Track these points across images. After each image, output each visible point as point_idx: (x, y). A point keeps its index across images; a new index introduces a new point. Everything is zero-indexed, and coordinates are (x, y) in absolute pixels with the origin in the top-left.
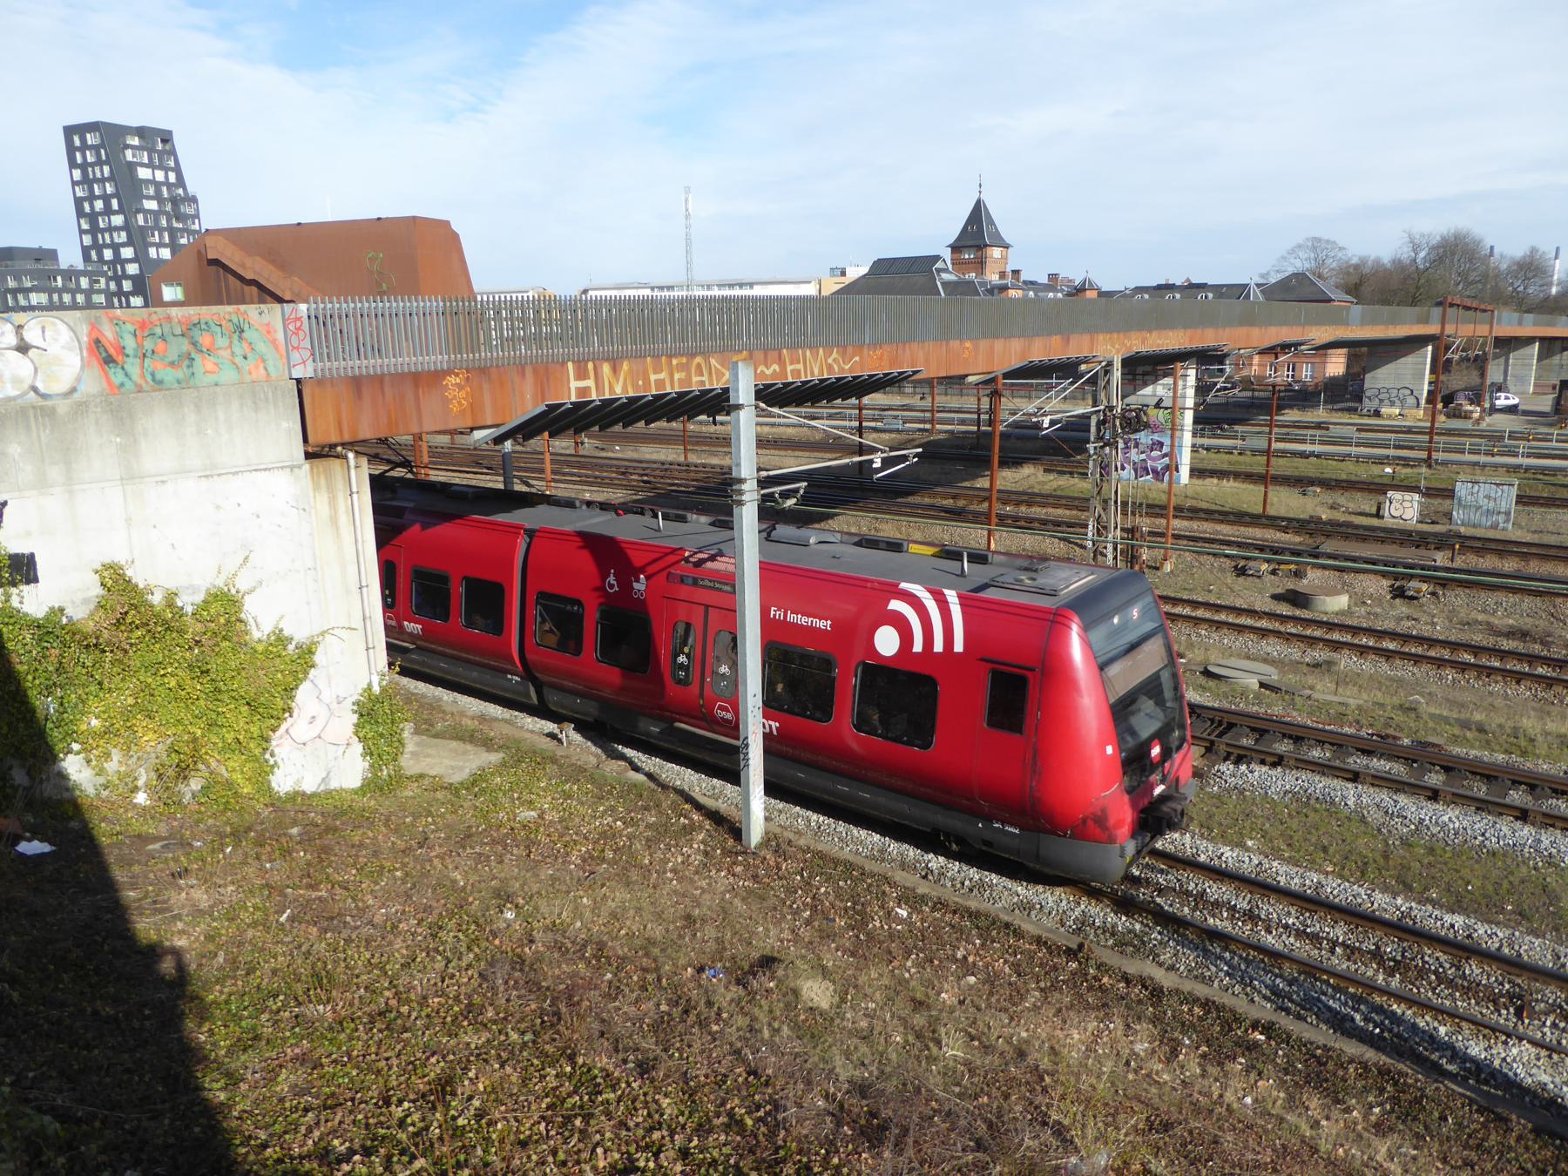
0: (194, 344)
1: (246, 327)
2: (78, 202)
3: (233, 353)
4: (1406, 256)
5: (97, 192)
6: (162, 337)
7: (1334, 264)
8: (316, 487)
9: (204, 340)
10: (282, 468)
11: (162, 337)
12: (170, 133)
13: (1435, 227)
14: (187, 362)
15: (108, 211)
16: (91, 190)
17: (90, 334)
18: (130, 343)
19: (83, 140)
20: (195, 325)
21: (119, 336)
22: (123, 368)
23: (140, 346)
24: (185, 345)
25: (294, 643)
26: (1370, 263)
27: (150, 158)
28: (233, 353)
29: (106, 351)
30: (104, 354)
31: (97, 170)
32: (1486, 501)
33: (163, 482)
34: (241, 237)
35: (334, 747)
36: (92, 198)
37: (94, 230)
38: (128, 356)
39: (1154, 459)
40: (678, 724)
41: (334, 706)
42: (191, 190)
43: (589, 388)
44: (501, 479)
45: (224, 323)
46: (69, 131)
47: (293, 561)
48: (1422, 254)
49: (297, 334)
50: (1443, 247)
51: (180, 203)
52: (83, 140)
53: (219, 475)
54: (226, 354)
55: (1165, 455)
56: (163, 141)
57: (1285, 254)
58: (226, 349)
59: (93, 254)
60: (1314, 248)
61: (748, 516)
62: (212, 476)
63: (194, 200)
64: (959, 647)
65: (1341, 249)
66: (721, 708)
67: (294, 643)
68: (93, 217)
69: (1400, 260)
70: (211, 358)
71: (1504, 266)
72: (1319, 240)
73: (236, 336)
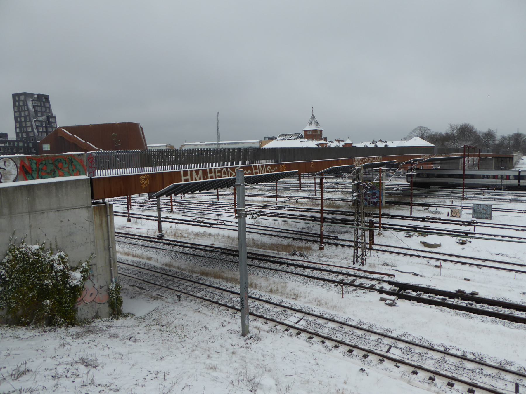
0: (56, 167)
1: (74, 161)
2: (16, 118)
3: (69, 169)
4: (450, 132)
5: (22, 114)
6: (45, 165)
7: (427, 135)
8: (95, 214)
9: (59, 165)
10: (84, 207)
11: (45, 165)
12: (48, 96)
13: (460, 121)
14: (53, 173)
17: (21, 164)
18: (34, 166)
20: (56, 160)
21: (31, 164)
22: (31, 175)
23: (38, 167)
24: (53, 167)
26: (438, 134)
27: (41, 104)
28: (69, 169)
29: (26, 169)
30: (25, 170)
31: (23, 107)
32: (483, 210)
33: (43, 213)
34: (73, 129)
35: (99, 304)
37: (21, 127)
38: (33, 171)
39: (373, 198)
41: (99, 289)
42: (54, 114)
43: (184, 176)
44: (126, 200)
45: (66, 159)
46: (14, 96)
47: (87, 239)
48: (455, 131)
49: (91, 163)
50: (461, 129)
51: (50, 120)
53: (62, 210)
54: (67, 169)
55: (377, 197)
56: (45, 98)
57: (411, 131)
58: (66, 168)
59: (20, 134)
60: (420, 130)
62: (60, 211)
63: (55, 117)
64: (97, 171)
65: (429, 130)
68: (20, 123)
69: (448, 133)
70: (62, 171)
71: (481, 135)
72: (422, 127)
73: (70, 164)
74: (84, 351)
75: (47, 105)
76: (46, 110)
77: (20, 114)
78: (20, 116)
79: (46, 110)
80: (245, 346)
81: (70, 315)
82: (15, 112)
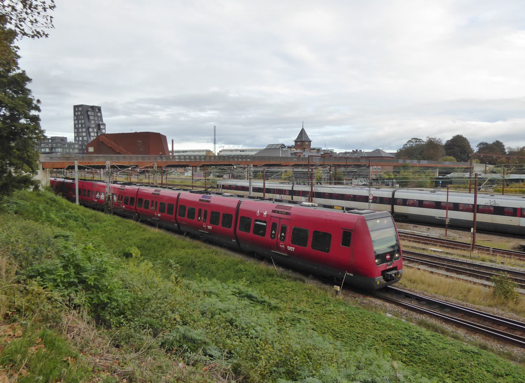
2: (75, 125)
12: (100, 107)
15: (82, 128)
16: (78, 122)
19: (78, 109)
25: (185, 234)
36: (78, 124)
40: (272, 251)
42: (104, 122)
51: (99, 126)
52: (78, 109)
61: (143, 203)
63: (104, 125)
66: (281, 244)
67: (185, 234)
74: (303, 329)
75: (99, 114)
76: (98, 119)
77: (78, 122)
78: (78, 124)
79: (98, 119)
80: (139, 261)
81: (312, 170)
82: (75, 120)
